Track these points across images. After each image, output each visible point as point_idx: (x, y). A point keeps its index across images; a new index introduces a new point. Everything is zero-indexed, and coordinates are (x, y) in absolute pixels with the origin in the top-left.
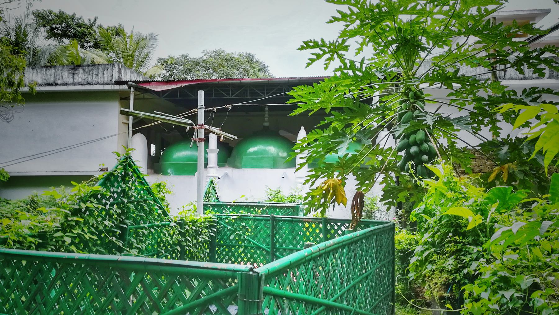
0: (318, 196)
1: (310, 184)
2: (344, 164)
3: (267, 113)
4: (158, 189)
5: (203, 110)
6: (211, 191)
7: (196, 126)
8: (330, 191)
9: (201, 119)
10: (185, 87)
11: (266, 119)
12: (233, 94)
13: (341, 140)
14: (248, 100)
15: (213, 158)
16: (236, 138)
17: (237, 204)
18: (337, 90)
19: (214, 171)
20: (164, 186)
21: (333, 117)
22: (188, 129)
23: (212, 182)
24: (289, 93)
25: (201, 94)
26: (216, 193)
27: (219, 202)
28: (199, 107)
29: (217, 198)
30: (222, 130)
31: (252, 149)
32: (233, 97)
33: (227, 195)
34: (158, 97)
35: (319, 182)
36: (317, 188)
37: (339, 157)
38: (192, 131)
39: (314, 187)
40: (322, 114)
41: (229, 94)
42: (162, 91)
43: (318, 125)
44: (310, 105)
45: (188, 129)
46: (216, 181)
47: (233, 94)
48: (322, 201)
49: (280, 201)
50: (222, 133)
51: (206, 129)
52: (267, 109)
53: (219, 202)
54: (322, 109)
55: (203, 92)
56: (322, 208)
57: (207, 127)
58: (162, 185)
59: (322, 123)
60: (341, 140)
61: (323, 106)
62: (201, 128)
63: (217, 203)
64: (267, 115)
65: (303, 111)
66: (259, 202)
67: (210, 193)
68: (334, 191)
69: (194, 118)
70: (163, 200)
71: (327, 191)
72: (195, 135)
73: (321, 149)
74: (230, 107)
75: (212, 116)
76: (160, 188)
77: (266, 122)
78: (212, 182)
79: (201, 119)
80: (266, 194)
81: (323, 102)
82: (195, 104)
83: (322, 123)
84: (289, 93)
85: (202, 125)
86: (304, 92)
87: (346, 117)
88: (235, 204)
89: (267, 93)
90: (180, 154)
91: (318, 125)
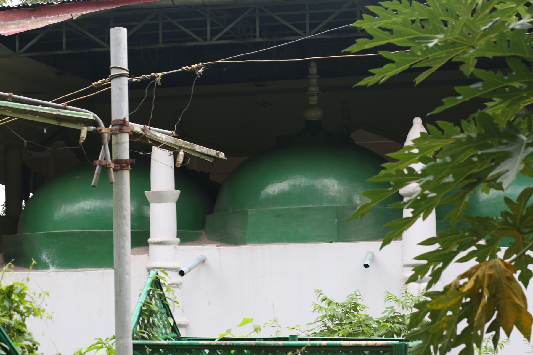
0: (450, 313)
1: (428, 276)
2: (523, 218)
3: (314, 84)
4: (6, 303)
5: (125, 81)
6: (155, 309)
7: (107, 126)
8: (481, 296)
9: (120, 108)
10: (83, 18)
11: (313, 100)
12: (214, 33)
13: (502, 149)
14: (259, 45)
15: (163, 218)
16: (222, 155)
17: (228, 342)
18: (494, 9)
19: (168, 252)
20: (22, 295)
21: (479, 85)
22: (84, 134)
23: (157, 284)
24: (358, 24)
25: (120, 38)
26: (169, 314)
27: (179, 338)
28: (113, 72)
29: (175, 329)
30: (181, 135)
31: (276, 188)
32: (214, 42)
33: (201, 319)
34: (9, 51)
35: (453, 272)
36: (446, 289)
37: (507, 200)
38: (95, 139)
39: (438, 287)
40: (451, 74)
41: (202, 34)
42: (21, 34)
43: (438, 110)
44: (417, 57)
45: (84, 134)
46: (167, 279)
47: (214, 33)
48: (463, 325)
49: (357, 334)
50: (181, 142)
51: (133, 135)
52: (313, 70)
53: (179, 338)
54: (452, 66)
55: (124, 31)
56: (463, 346)
57: (138, 128)
58: (16, 291)
59: (449, 103)
60: (502, 149)
61: (455, 55)
62: (121, 131)
63: (174, 341)
64: (314, 89)
65: (400, 70)
66: (293, 338)
67: (152, 313)
68: (492, 296)
69: (102, 104)
70: (20, 333)
71: (475, 294)
72: (105, 151)
73: (450, 179)
74: (199, 68)
75: (149, 99)
76: (12, 301)
77: (312, 107)
78: (157, 284)
79: (120, 108)
80: (318, 314)
81: (453, 44)
82: (102, 66)
83: (449, 103)
84: (358, 24)
85: (122, 124)
86: (398, 19)
87: (517, 85)
88: (223, 342)
89: (313, 26)
90: (74, 207)
91: (438, 110)
